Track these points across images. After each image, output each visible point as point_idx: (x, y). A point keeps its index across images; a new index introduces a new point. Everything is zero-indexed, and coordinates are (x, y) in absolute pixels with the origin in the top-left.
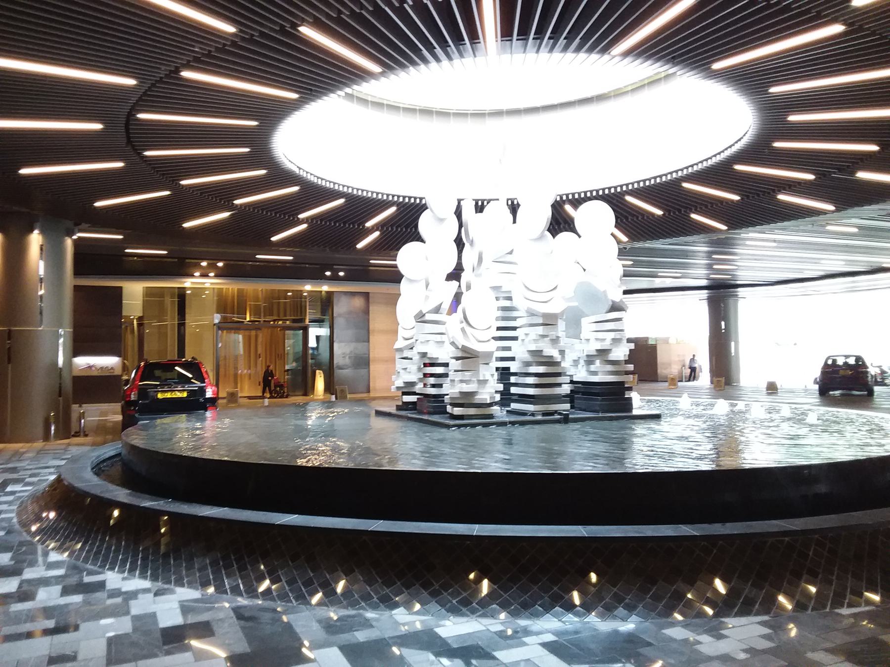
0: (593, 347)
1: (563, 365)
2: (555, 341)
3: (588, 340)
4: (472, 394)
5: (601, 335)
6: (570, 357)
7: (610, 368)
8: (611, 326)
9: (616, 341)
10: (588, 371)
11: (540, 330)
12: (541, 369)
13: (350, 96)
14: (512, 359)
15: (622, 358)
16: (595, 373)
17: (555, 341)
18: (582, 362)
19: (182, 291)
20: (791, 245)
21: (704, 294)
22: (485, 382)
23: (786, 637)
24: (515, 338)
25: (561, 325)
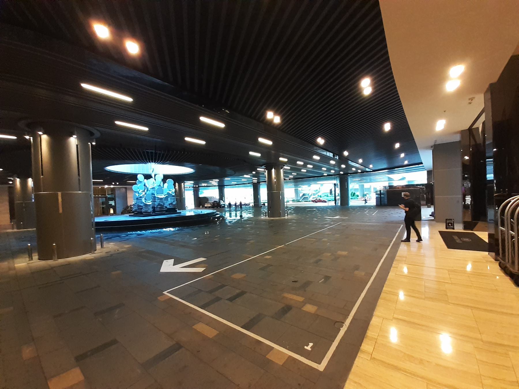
17: (162, 202)
22: (149, 209)
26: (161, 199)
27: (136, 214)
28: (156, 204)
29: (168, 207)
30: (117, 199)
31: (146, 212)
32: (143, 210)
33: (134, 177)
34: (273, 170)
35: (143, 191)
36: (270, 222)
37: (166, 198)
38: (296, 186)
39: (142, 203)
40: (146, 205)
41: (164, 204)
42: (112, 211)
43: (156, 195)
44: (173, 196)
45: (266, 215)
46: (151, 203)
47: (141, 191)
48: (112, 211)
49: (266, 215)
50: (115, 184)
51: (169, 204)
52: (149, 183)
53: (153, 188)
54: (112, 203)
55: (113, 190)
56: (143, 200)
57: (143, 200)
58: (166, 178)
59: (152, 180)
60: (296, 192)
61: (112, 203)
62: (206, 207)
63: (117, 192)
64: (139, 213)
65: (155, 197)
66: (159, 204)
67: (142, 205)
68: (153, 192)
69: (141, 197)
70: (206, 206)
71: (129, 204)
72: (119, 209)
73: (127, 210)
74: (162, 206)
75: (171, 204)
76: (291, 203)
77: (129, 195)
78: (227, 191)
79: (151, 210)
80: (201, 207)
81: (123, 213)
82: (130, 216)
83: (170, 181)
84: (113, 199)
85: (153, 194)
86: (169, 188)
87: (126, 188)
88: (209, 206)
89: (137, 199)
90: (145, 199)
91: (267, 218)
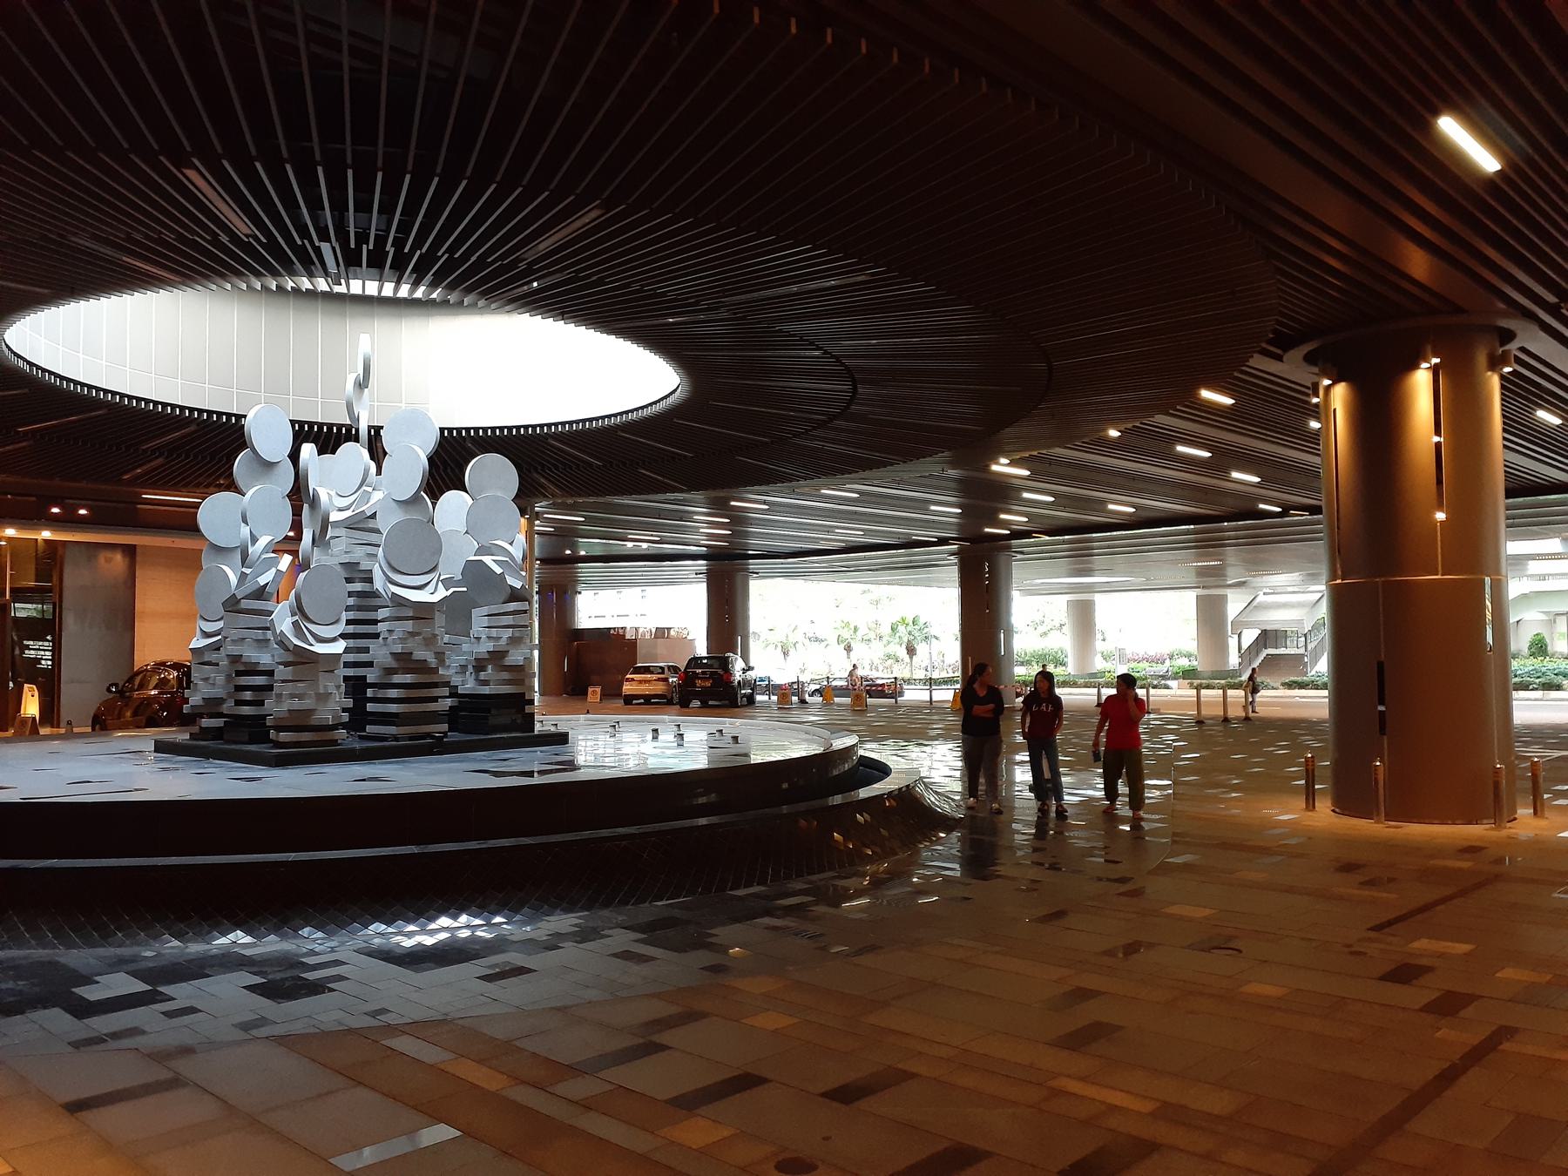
0: (485, 647)
3: (478, 639)
4: (311, 712)
5: (494, 632)
6: (454, 660)
7: (505, 675)
8: (508, 620)
11: (409, 625)
12: (408, 678)
14: (370, 664)
16: (485, 683)
17: (430, 641)
18: (470, 669)
22: (324, 697)
24: (376, 636)
26: (423, 612)
27: (216, 734)
28: (380, 653)
29: (468, 685)
30: (70, 624)
31: (299, 722)
32: (275, 707)
33: (205, 447)
34: (1421, 381)
35: (279, 548)
36: (1350, 863)
37: (457, 610)
38: (1211, 577)
39: (263, 643)
40: (303, 660)
41: (440, 656)
42: (31, 706)
43: (379, 583)
44: (515, 595)
45: (1310, 795)
46: (339, 647)
47: (264, 541)
48: (31, 706)
49: (1310, 795)
50: (67, 521)
51: (480, 665)
52: (336, 479)
53: (361, 524)
54: (39, 651)
55: (50, 560)
56: (283, 621)
57: (283, 621)
58: (451, 458)
59: (354, 454)
60: (1211, 617)
61: (39, 651)
62: (628, 700)
63: (74, 578)
64: (239, 733)
65: (367, 599)
66: (405, 661)
67: (265, 659)
68: (359, 554)
69: (261, 593)
70: (628, 688)
71: (138, 664)
72: (83, 689)
73: (138, 703)
74: (424, 678)
75: (497, 656)
76: (1179, 691)
77: (155, 596)
78: (770, 600)
79: (334, 705)
80: (594, 693)
81: (103, 722)
82: (161, 747)
83: (494, 475)
84: (46, 628)
85: (354, 572)
86: (482, 525)
87: (130, 551)
88: (659, 688)
89: (232, 605)
90: (299, 609)
91: (1324, 815)
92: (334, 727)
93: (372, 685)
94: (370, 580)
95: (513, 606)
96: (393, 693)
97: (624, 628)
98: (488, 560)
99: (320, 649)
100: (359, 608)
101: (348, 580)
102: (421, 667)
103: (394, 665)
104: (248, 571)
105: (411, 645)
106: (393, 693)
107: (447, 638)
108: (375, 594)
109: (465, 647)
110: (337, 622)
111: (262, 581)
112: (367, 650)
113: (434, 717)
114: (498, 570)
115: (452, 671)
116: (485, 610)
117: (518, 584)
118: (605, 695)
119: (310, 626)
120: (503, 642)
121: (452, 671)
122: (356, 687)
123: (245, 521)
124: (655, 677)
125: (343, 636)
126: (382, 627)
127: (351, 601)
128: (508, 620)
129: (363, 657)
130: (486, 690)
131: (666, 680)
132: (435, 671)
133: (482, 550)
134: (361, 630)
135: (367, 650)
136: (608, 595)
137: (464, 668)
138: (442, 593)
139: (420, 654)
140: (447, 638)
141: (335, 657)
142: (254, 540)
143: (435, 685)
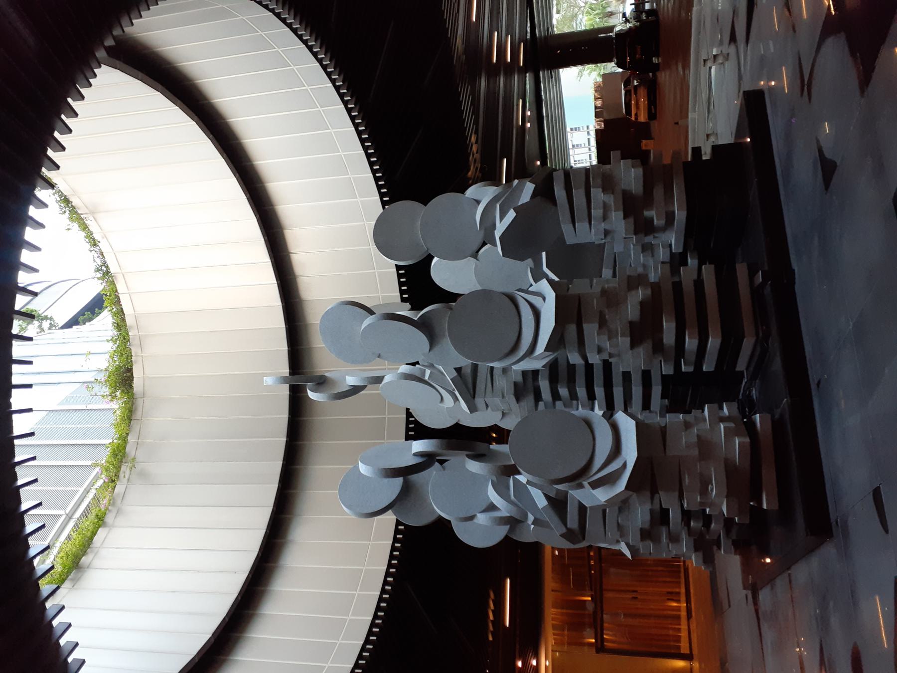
0: (618, 222)
1: (653, 277)
2: (611, 299)
3: (607, 233)
4: (730, 469)
5: (597, 212)
6: (635, 259)
7: (658, 193)
8: (579, 196)
9: (608, 184)
10: (664, 229)
11: (590, 329)
12: (669, 328)
13: (74, 566)
14: (646, 376)
15: (640, 171)
16: (670, 218)
17: (611, 299)
18: (649, 239)
19: (492, 368)
20: (495, 19)
21: (14, 408)
22: (705, 447)
23: (101, 54)
24: (607, 366)
25: (579, 286)
26: (570, 310)
28: (631, 360)
37: (570, 263)
41: (635, 282)
46: (628, 425)
47: (493, 496)
51: (643, 228)
62: (652, 116)
66: (643, 331)
68: (503, 383)
70: (642, 118)
75: (632, 206)
79: (714, 426)
88: (642, 92)
92: (750, 427)
93: (677, 366)
94: (535, 373)
95: (559, 192)
96: (691, 343)
97: (596, 130)
98: (501, 228)
99: (630, 453)
100: (571, 382)
101: (538, 397)
102: (651, 313)
103: (648, 345)
104: (531, 518)
105: (618, 324)
106: (691, 343)
107: (607, 273)
108: (553, 367)
109: (618, 248)
110: (588, 424)
111: (541, 502)
112: (627, 376)
113: (727, 283)
114: (511, 215)
115: (651, 262)
116: (566, 228)
117: (529, 188)
118: (649, 136)
119: (599, 461)
120: (610, 199)
121: (651, 262)
122: (684, 392)
123: (472, 518)
124: (633, 96)
125: (609, 414)
126: (595, 359)
127: (563, 391)
128: (579, 196)
129: (636, 379)
130: (680, 215)
131: (636, 87)
132: (656, 288)
133: (488, 239)
134: (603, 384)
135: (627, 376)
136: (573, 138)
137: (647, 248)
138: (544, 286)
139: (631, 309)
140: (607, 273)
141: (642, 430)
142: (492, 507)
143: (677, 287)
